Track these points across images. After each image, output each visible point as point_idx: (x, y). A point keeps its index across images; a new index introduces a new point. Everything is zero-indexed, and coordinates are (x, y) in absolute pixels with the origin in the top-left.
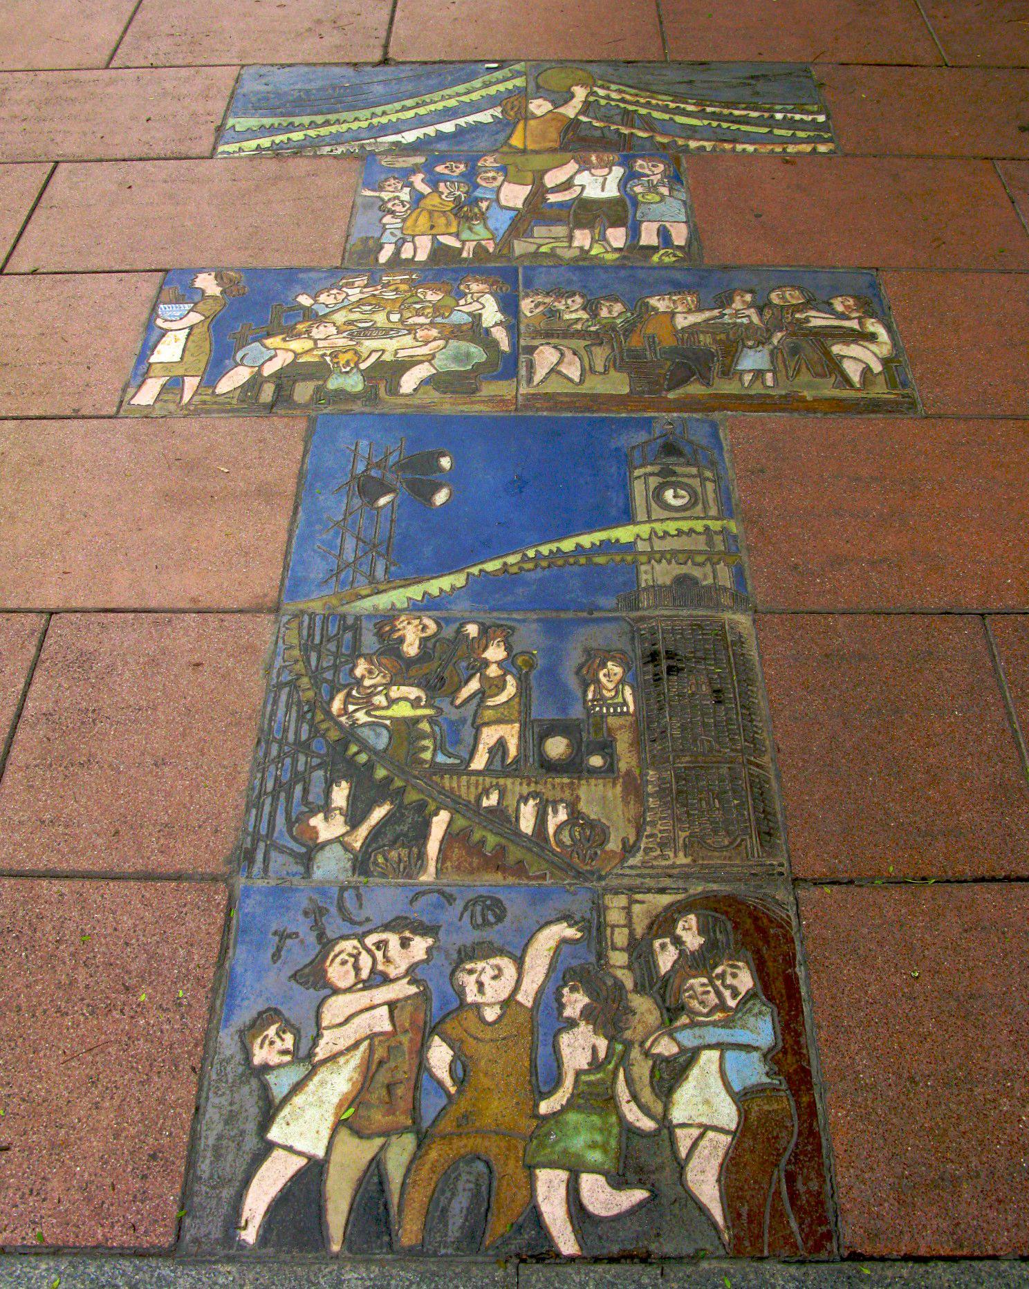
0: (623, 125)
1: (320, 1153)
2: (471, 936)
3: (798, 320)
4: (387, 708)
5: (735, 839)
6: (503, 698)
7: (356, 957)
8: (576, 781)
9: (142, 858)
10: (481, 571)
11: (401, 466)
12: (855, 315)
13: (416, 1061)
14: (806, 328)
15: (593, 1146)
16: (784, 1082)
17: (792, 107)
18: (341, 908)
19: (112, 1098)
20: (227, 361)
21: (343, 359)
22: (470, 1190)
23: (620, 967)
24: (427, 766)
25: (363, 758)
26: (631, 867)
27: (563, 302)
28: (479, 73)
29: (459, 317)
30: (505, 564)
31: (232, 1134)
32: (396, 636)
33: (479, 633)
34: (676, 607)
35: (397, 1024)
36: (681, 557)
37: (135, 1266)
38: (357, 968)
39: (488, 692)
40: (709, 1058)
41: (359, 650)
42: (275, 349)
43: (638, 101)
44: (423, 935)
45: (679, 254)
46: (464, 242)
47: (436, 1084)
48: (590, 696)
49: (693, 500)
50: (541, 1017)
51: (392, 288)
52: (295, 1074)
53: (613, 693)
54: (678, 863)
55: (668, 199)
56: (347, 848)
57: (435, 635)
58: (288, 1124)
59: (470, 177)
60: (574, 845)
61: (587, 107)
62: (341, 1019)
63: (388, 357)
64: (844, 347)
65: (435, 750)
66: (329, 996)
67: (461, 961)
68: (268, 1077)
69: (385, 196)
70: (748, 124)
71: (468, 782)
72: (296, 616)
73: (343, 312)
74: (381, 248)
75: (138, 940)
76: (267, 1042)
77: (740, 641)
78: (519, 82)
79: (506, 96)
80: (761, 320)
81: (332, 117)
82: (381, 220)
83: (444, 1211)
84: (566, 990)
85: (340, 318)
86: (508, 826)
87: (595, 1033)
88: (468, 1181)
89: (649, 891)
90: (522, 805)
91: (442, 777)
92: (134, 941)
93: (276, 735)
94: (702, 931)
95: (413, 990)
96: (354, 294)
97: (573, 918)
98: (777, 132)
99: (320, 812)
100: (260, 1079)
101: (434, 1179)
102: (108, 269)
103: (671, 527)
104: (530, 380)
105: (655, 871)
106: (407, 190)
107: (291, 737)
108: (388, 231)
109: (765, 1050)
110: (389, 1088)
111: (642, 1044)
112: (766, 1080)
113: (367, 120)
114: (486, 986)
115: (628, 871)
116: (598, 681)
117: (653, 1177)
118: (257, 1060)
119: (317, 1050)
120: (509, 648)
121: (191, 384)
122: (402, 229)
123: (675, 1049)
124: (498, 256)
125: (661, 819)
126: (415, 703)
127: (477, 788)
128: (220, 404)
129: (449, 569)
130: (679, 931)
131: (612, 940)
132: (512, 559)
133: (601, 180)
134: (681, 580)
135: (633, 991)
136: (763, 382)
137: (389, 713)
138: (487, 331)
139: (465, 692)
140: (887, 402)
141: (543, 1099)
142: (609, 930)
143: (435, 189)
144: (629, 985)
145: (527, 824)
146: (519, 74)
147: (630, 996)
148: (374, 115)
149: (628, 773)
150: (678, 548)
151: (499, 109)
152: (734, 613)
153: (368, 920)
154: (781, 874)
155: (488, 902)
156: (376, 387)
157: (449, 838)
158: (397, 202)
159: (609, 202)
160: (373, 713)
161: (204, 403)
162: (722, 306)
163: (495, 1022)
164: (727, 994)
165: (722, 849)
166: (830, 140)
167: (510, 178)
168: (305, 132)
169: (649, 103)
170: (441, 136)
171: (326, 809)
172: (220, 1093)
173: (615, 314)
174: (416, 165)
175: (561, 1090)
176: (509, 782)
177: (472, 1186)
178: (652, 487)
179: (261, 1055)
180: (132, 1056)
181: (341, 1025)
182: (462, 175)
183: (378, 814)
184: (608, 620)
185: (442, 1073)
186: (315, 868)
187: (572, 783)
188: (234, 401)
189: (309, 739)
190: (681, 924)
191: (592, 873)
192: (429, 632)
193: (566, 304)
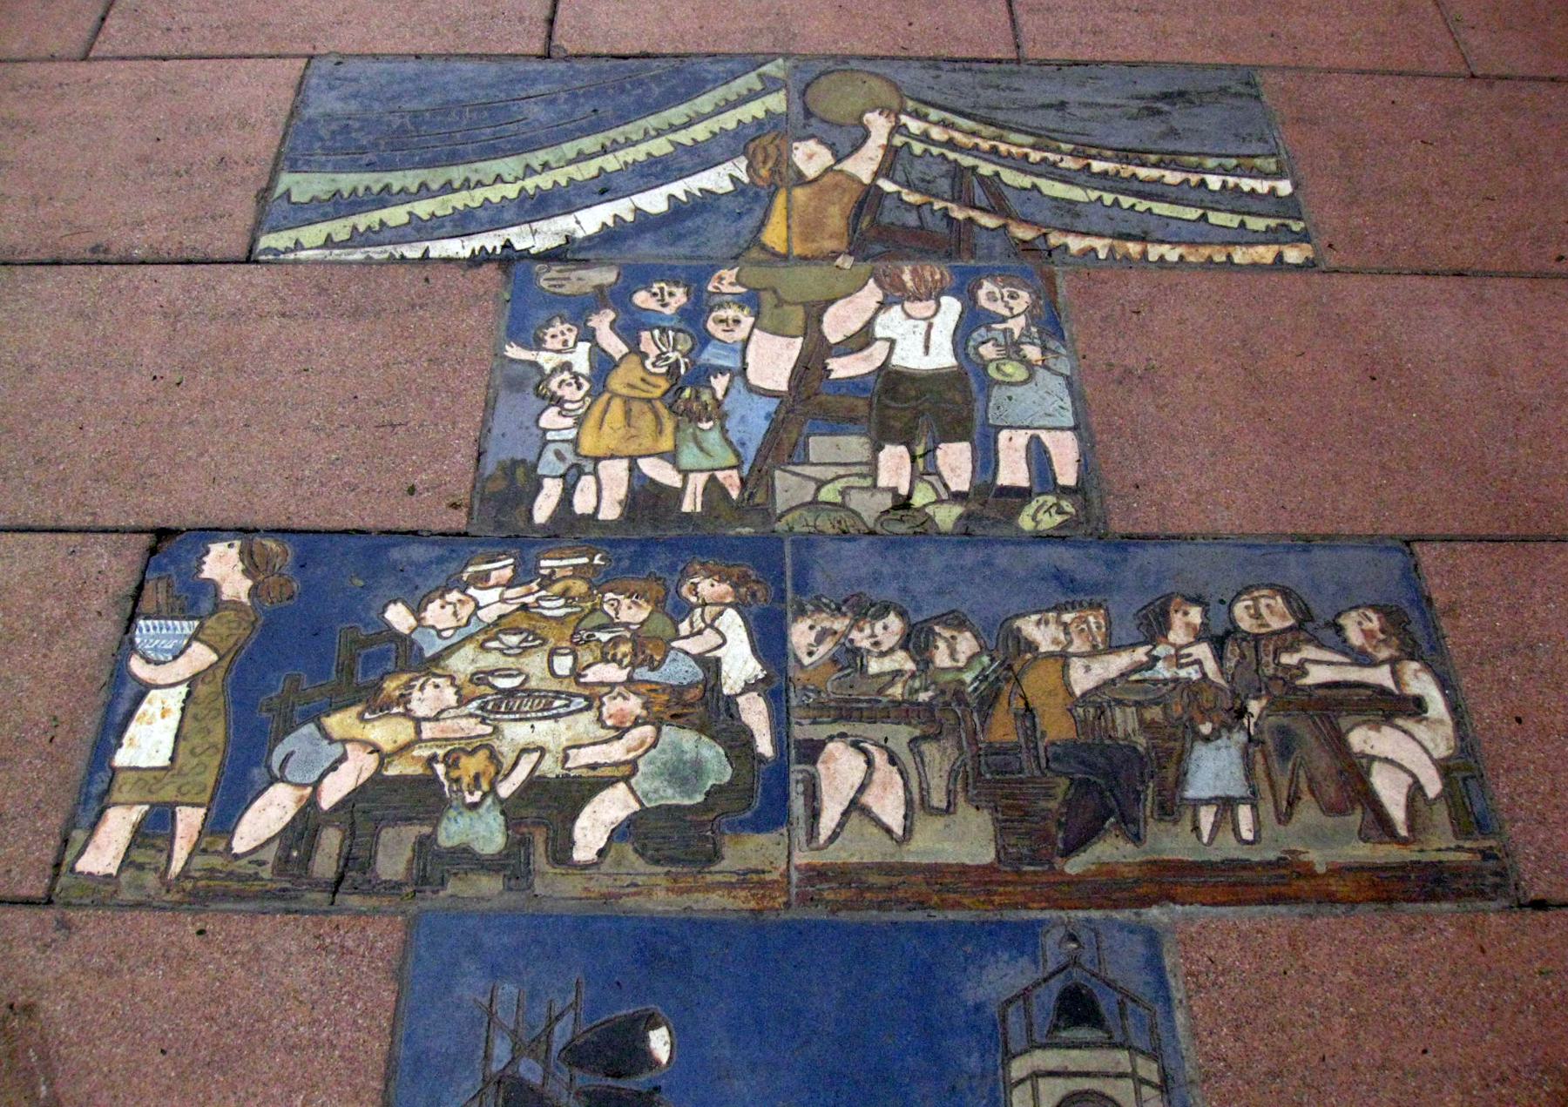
0: (953, 201)
3: (1287, 667)
12: (1384, 653)
14: (1302, 688)
17: (1234, 162)
20: (256, 771)
21: (471, 765)
27: (868, 631)
28: (705, 81)
29: (678, 670)
42: (344, 741)
43: (976, 147)
45: (1067, 505)
46: (685, 473)
51: (558, 588)
55: (1041, 373)
59: (694, 317)
61: (893, 159)
63: (550, 768)
64: (1372, 734)
69: (547, 360)
70: (1160, 198)
73: (469, 650)
74: (539, 487)
78: (776, 102)
79: (751, 131)
80: (1222, 672)
81: (457, 173)
82: (537, 421)
85: (463, 663)
96: (491, 602)
98: (1215, 218)
102: (50, 524)
104: (812, 832)
106: (584, 347)
108: (552, 447)
113: (517, 179)
121: (189, 820)
122: (575, 442)
124: (742, 509)
133: (923, 325)
136: (1236, 831)
138: (731, 700)
140: (1458, 871)
143: (634, 348)
146: (770, 85)
148: (529, 171)
151: (742, 163)
156: (526, 842)
158: (566, 376)
159: (936, 377)
161: (211, 872)
162: (1152, 640)
166: (1303, 237)
167: (765, 321)
168: (408, 207)
169: (994, 150)
170: (644, 223)
173: (962, 660)
174: (600, 288)
182: (682, 311)
188: (266, 873)
193: (873, 635)
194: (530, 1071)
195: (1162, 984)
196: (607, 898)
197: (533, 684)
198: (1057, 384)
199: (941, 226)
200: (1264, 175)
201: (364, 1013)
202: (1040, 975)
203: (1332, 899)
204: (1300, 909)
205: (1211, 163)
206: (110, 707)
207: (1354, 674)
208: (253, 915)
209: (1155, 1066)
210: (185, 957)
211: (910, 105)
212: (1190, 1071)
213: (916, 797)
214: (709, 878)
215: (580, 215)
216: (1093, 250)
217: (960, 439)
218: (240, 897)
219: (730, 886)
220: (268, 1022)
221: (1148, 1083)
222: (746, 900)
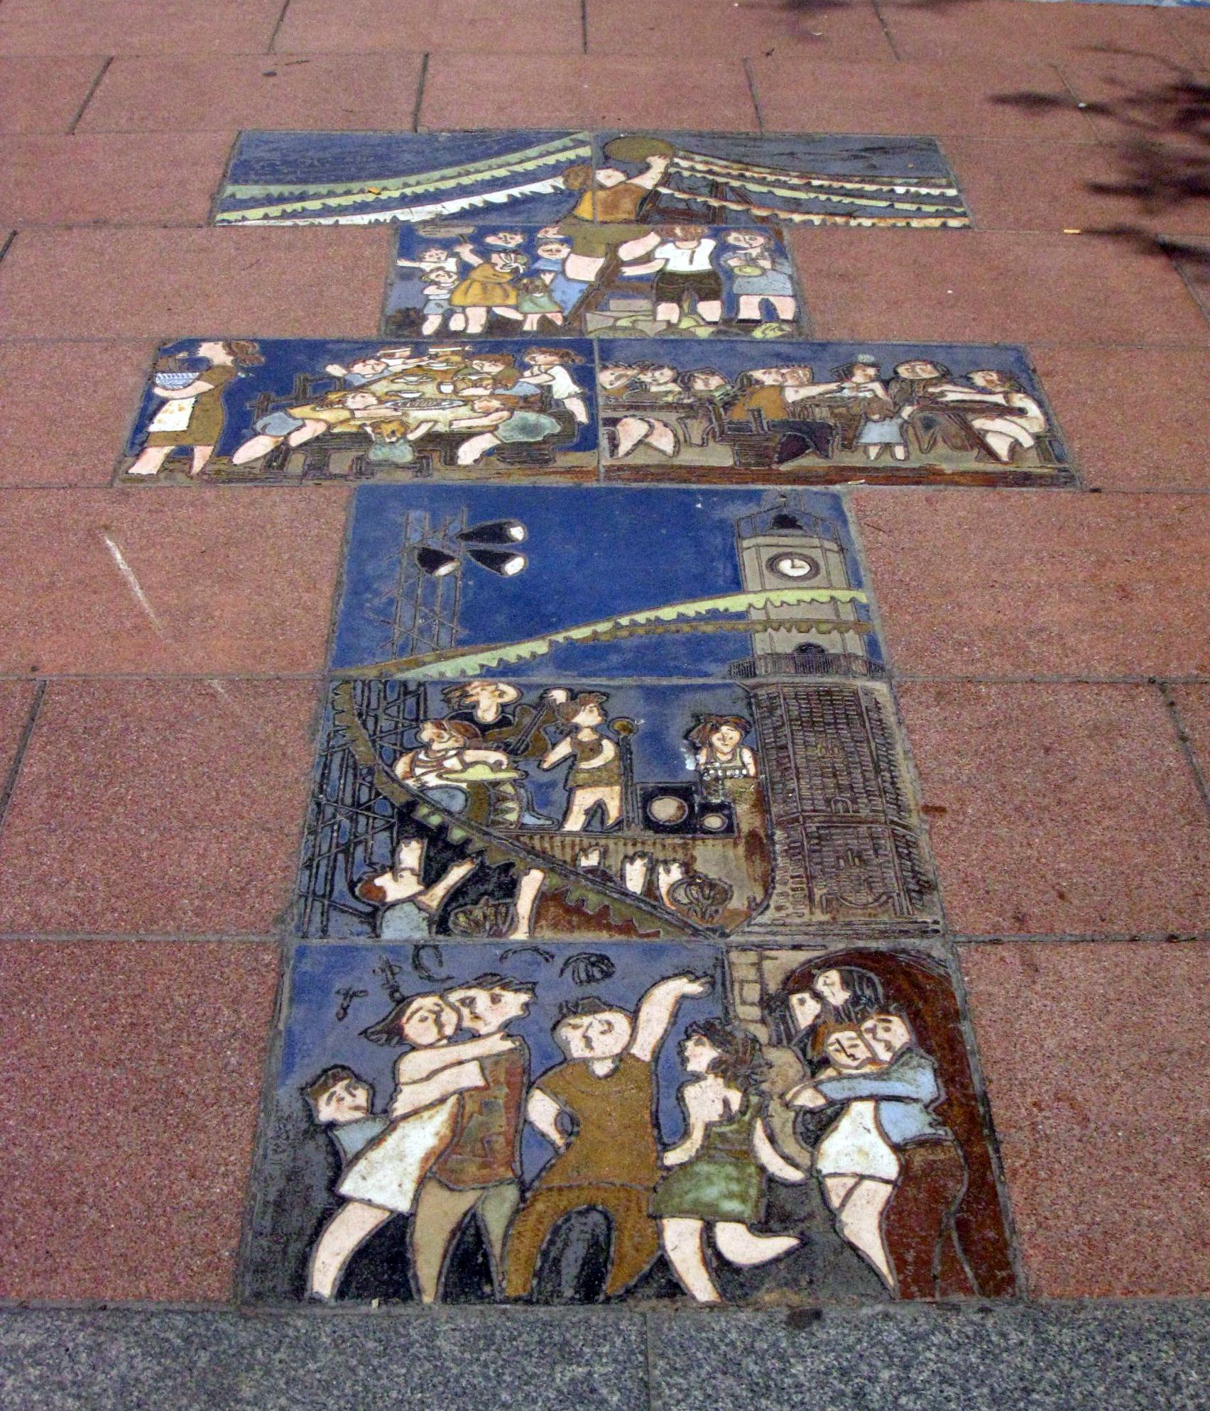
1: (404, 1206)
7: (438, 1014)
10: (566, 638)
15: (730, 1196)
16: (950, 1132)
26: (761, 925)
38: (439, 1024)
52: (375, 1128)
59: (529, 248)
61: (666, 179)
62: (424, 1075)
66: (406, 1053)
67: (564, 1016)
73: (384, 383)
76: (334, 1098)
83: (557, 1261)
88: (582, 1231)
89: (781, 947)
92: (168, 1001)
94: (846, 984)
95: (508, 1045)
96: (396, 365)
98: (898, 206)
111: (782, 1096)
112: (929, 1130)
114: (594, 1039)
115: (756, 929)
116: (711, 745)
119: (397, 1105)
120: (604, 713)
122: (449, 300)
126: (496, 766)
134: (804, 649)
142: (737, 986)
146: (582, 143)
154: (937, 931)
170: (490, 208)
171: (393, 867)
189: (370, 800)
197: (427, 396)
198: (783, 278)
199: (705, 210)
200: (939, 186)
204: (934, 487)
205: (899, 181)
206: (144, 409)
207: (978, 397)
210: (206, 504)
211: (681, 153)
213: (682, 438)
215: (445, 204)
216: (812, 221)
217: (715, 299)
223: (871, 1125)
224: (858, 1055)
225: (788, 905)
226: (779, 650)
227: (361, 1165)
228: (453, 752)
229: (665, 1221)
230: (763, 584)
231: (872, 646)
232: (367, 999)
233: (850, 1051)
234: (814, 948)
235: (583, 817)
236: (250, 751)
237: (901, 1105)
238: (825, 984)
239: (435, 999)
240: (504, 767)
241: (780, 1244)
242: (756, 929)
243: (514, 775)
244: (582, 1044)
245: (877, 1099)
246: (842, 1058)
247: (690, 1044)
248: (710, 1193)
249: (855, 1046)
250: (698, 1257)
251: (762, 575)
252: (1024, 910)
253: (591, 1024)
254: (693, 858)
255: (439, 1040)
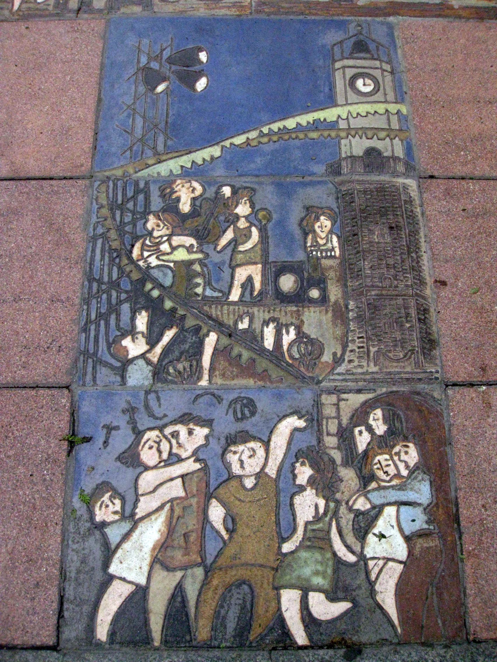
1: (143, 581)
2: (233, 428)
4: (171, 253)
5: (407, 354)
6: (248, 245)
7: (158, 443)
8: (301, 309)
9: (11, 372)
10: (231, 144)
11: (170, 61)
13: (201, 517)
15: (317, 573)
16: (436, 528)
18: (147, 407)
19: (7, 546)
22: (239, 605)
23: (333, 448)
24: (200, 298)
25: (155, 293)
26: (339, 374)
30: (248, 138)
31: (86, 569)
32: (174, 196)
33: (232, 194)
34: (366, 173)
35: (188, 492)
36: (370, 133)
37: (33, 656)
38: (160, 452)
39: (240, 240)
40: (390, 511)
41: (149, 209)
44: (202, 426)
47: (215, 534)
48: (309, 244)
49: (376, 89)
50: (281, 485)
52: (126, 526)
53: (324, 241)
54: (370, 370)
56: (149, 362)
57: (201, 195)
58: (121, 563)
60: (301, 357)
62: (151, 489)
65: (204, 286)
66: (141, 473)
67: (229, 445)
68: (106, 530)
71: (228, 310)
72: (103, 182)
75: (13, 434)
76: (104, 506)
77: (410, 201)
83: (224, 618)
84: (298, 465)
86: (256, 343)
87: (317, 495)
88: (238, 598)
89: (350, 391)
90: (265, 327)
91: (210, 307)
92: (10, 434)
93: (95, 276)
94: (385, 420)
95: (198, 466)
97: (300, 412)
99: (129, 335)
100: (101, 532)
101: (217, 598)
103: (362, 109)
105: (354, 377)
107: (106, 279)
109: (426, 505)
110: (186, 536)
111: (347, 503)
112: (425, 526)
114: (245, 462)
115: (337, 377)
116: (314, 231)
117: (354, 593)
118: (98, 519)
119: (137, 511)
120: (252, 206)
123: (368, 506)
125: (359, 338)
126: (189, 249)
127: (234, 315)
128: (40, 10)
129: (209, 142)
130: (371, 422)
131: (327, 428)
132: (253, 135)
134: (370, 152)
135: (341, 465)
137: (171, 257)
139: (223, 241)
141: (285, 542)
142: (324, 422)
144: (339, 461)
145: (269, 343)
147: (339, 469)
149: (336, 303)
150: (367, 126)
152: (406, 178)
153: (165, 416)
154: (437, 378)
155: (245, 401)
157: (216, 352)
160: (161, 258)
161: (29, 9)
163: (252, 489)
164: (401, 466)
165: (398, 361)
171: (132, 332)
172: (76, 541)
175: (296, 536)
176: (255, 309)
177: (241, 602)
178: (348, 77)
179: (100, 515)
180: (17, 517)
181: (151, 492)
183: (169, 335)
184: (319, 183)
185: (219, 525)
186: (128, 379)
187: (298, 311)
188: (51, 8)
189: (119, 278)
190: (372, 416)
191: (312, 378)
192: (198, 193)
194: (155, 65)
195: (394, 41)
196: (182, 12)
201: (91, 50)
202: (347, 36)
203: (460, 17)
204: (447, 20)
208: (47, 22)
209: (389, 66)
210: (22, 35)
212: (402, 68)
214: (221, 5)
218: (41, 16)
219: (229, 7)
220: (55, 55)
221: (386, 71)
222: (235, 12)
223: (394, 524)
224: (389, 472)
225: (355, 359)
226: (355, 154)
227: (119, 553)
228: (165, 238)
229: (282, 591)
230: (346, 100)
231: (409, 150)
232: (119, 432)
233: (385, 469)
234: (369, 390)
235: (240, 289)
236: (50, 239)
237: (411, 508)
238: (374, 420)
239: (156, 432)
240: (195, 250)
241: (343, 606)
242: (337, 377)
243: (200, 256)
244: (238, 466)
245: (400, 504)
246: (380, 474)
247: (298, 465)
248: (307, 571)
249: (388, 465)
250: (299, 616)
251: (346, 92)
252: (487, 362)
253: (244, 450)
254: (302, 322)
255: (160, 462)
